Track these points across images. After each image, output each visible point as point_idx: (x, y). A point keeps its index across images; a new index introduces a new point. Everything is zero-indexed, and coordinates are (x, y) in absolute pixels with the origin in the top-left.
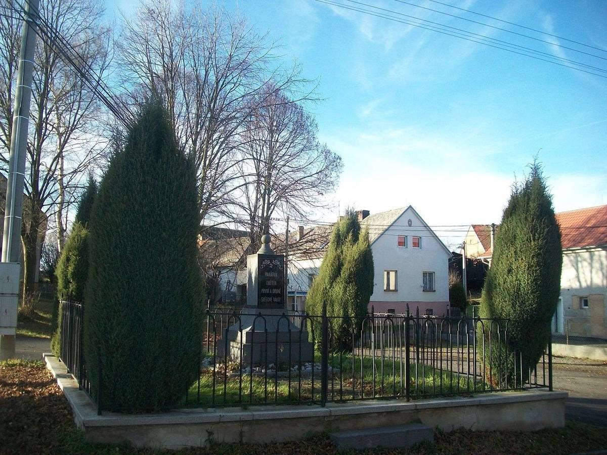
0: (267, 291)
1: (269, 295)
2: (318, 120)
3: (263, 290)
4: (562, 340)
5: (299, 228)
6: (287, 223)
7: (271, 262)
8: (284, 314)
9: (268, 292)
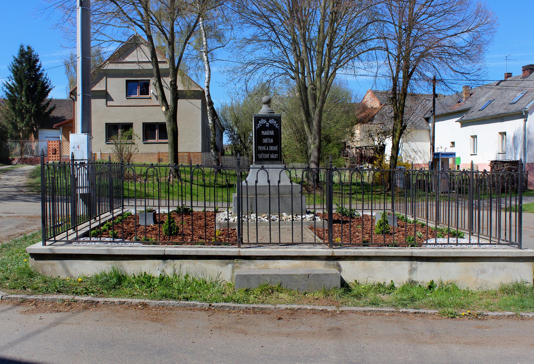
0: (264, 148)
1: (266, 152)
2: (53, 84)
3: (260, 148)
4: (515, 157)
5: (464, 89)
6: (436, 92)
7: (268, 121)
8: (285, 167)
9: (265, 149)
